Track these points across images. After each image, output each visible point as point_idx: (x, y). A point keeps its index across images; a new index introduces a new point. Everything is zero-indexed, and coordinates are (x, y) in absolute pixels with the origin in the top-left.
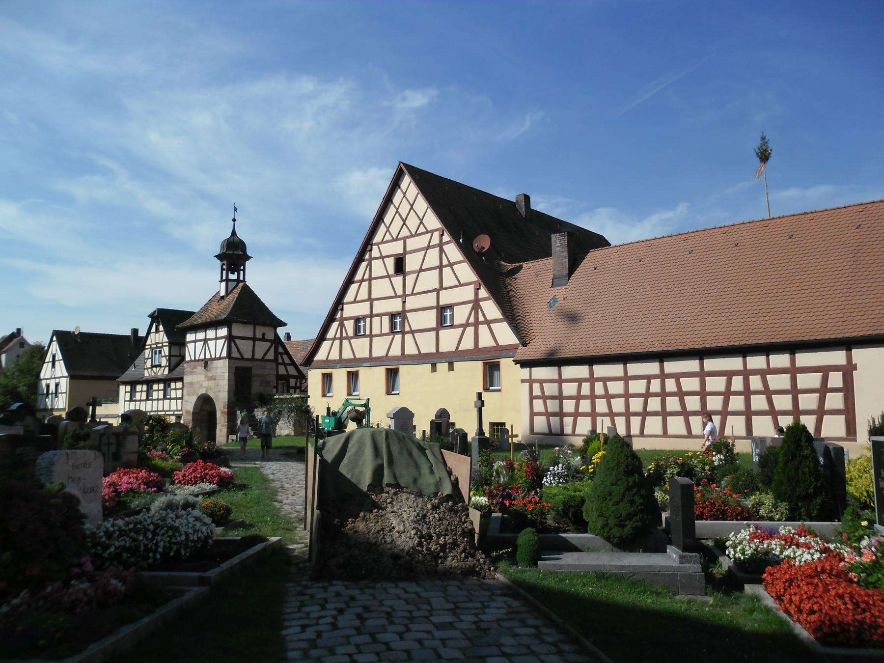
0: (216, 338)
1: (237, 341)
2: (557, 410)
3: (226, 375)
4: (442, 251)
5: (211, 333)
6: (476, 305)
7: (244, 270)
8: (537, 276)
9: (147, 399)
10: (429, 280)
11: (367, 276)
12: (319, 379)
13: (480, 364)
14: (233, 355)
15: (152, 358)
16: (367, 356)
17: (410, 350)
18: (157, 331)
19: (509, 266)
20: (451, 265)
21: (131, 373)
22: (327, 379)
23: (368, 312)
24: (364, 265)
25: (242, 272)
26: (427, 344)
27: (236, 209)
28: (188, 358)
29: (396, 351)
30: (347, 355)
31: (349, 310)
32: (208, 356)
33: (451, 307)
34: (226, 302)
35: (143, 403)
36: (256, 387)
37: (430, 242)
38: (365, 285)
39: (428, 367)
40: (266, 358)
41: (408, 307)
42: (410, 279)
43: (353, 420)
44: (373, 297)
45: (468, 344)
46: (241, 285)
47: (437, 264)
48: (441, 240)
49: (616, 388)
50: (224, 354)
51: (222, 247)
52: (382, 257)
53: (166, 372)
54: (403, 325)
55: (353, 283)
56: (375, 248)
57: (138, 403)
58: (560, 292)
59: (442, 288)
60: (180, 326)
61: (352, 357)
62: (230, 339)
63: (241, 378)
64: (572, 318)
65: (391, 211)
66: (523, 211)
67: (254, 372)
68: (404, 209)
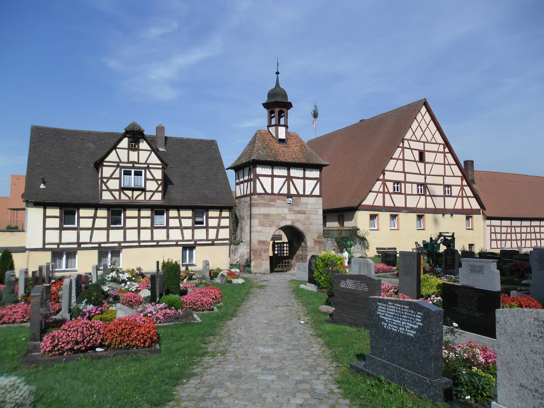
0: (304, 178)
4: (445, 156)
6: (462, 189)
12: (389, 217)
17: (430, 205)
30: (389, 203)
39: (464, 216)
40: (281, 192)
45: (459, 206)
49: (518, 230)
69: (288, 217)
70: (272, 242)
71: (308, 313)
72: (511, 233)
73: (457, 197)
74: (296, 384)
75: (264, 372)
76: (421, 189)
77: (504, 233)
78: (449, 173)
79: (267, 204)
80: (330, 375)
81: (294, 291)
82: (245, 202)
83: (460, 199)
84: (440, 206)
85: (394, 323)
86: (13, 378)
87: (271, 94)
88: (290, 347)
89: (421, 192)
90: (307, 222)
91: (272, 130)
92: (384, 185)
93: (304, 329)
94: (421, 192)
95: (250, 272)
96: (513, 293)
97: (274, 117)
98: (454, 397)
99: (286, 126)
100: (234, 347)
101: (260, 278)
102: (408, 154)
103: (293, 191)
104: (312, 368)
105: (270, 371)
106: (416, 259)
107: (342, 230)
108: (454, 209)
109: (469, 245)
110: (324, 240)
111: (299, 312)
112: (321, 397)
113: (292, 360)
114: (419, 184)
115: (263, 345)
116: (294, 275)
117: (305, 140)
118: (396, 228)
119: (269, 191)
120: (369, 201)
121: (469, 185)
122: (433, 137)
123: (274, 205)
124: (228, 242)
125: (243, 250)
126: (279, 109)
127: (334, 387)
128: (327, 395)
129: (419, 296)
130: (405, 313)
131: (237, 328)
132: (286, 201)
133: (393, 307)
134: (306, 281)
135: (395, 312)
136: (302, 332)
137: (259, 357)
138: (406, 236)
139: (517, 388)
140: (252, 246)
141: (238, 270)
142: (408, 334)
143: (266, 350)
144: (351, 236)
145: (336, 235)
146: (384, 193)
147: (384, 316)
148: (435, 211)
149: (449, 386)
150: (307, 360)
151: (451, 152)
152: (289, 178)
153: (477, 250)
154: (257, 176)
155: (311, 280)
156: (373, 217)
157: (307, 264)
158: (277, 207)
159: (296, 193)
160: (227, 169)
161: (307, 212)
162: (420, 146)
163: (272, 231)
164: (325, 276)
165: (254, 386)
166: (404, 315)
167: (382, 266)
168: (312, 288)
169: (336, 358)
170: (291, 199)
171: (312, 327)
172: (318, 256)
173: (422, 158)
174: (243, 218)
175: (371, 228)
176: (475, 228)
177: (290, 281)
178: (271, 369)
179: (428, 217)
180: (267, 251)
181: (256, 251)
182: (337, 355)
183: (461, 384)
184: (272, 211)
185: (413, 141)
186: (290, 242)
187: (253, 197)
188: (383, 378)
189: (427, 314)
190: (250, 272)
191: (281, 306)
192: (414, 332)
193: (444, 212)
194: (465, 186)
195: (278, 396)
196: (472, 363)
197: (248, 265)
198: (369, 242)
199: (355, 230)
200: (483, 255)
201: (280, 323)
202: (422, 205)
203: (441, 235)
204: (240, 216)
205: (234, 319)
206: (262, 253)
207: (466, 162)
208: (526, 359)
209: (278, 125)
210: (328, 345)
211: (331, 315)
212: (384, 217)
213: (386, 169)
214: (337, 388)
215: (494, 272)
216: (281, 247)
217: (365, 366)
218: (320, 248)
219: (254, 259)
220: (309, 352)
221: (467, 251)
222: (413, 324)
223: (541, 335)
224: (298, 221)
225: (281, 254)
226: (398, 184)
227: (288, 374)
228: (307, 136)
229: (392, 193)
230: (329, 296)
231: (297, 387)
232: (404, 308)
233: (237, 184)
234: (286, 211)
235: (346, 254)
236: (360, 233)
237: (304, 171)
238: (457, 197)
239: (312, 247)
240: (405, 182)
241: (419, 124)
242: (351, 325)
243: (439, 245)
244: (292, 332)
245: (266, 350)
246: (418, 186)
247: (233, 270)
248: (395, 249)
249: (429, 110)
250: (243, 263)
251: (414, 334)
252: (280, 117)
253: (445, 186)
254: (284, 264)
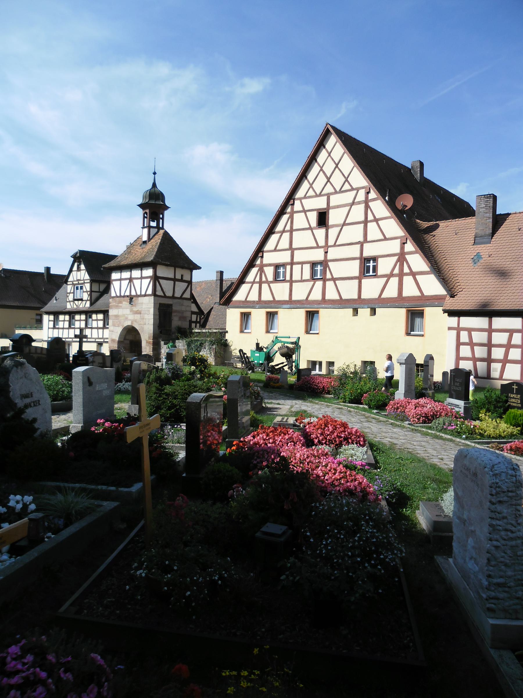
0: (142, 278)
1: (161, 281)
2: (485, 356)
3: (152, 311)
4: (367, 207)
5: (136, 273)
6: (402, 257)
7: (163, 219)
8: (456, 234)
9: (70, 327)
10: (355, 233)
11: (288, 228)
12: (238, 316)
13: (403, 311)
14: (157, 293)
15: (74, 293)
16: (287, 298)
17: (331, 294)
18: (79, 269)
19: (425, 225)
20: (376, 220)
21: (53, 304)
22: (245, 317)
23: (289, 260)
24: (285, 217)
25: (161, 220)
26: (349, 291)
28: (113, 294)
29: (316, 295)
30: (266, 296)
31: (269, 258)
32: (133, 293)
33: (375, 259)
34: (149, 246)
35: (66, 331)
36: (176, 322)
37: (355, 198)
38: (286, 235)
41: (329, 257)
42: (333, 233)
43: (283, 355)
44: (294, 247)
45: (391, 292)
46: (161, 232)
47: (362, 219)
48: (367, 197)
50: (150, 291)
51: (144, 197)
52: (305, 211)
53: (88, 304)
54: (324, 272)
55: (274, 233)
56: (297, 203)
57: (61, 331)
58: (484, 249)
59: (366, 240)
60: (106, 265)
61: (272, 299)
62: (156, 279)
63: (164, 313)
64: (502, 274)
65: (315, 169)
66: (418, 176)
67: (174, 308)
68: (329, 167)
86: (387, 507)
90: (142, 323)
173: (323, 219)
229: (271, 282)
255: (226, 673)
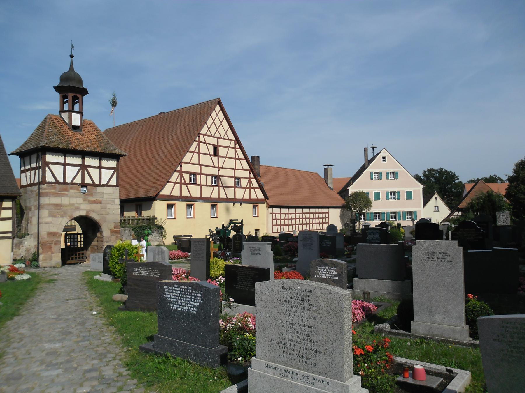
1: (50, 166)
4: (236, 151)
6: (250, 181)
16: (199, 196)
17: (223, 196)
27: (73, 47)
30: (185, 193)
39: (251, 205)
40: (74, 182)
45: (247, 197)
69: (83, 207)
70: (64, 233)
71: (102, 304)
72: (316, 218)
73: (246, 188)
74: (84, 374)
75: (49, 368)
76: (215, 180)
77: (283, 219)
78: (239, 166)
79: (58, 194)
80: (120, 360)
81: (87, 283)
82: (32, 191)
83: (248, 190)
84: (231, 196)
85: (179, 303)
87: (64, 78)
88: (80, 339)
89: (215, 183)
91: (65, 116)
92: (181, 176)
93: (96, 319)
94: (215, 183)
95: (38, 267)
96: (285, 269)
97: (67, 102)
98: (229, 361)
99: (81, 113)
100: (14, 348)
101: (50, 271)
102: (203, 148)
103: (88, 181)
104: (101, 356)
105: (57, 366)
106: (206, 244)
107: (139, 220)
108: (243, 199)
109: (255, 230)
110: (121, 229)
111: (92, 303)
112: (109, 382)
113: (81, 351)
114: (213, 176)
115: (50, 341)
116: (88, 266)
117: (102, 129)
118: (192, 217)
119: (61, 180)
120: (166, 191)
121: (255, 178)
122: (226, 134)
123: (67, 194)
124: (10, 235)
125: (29, 244)
126: (73, 95)
127: (123, 370)
128: (116, 379)
129: (208, 277)
130: (189, 294)
131: (18, 328)
132: (80, 191)
133: (178, 289)
134: (100, 272)
135: (180, 294)
136: (93, 323)
137: (44, 354)
138: (200, 224)
139: (269, 343)
140: (40, 238)
141: (23, 266)
142: (191, 312)
143: (52, 346)
144: (148, 225)
145: (133, 224)
146: (181, 183)
147: (170, 298)
148: (227, 200)
149: (224, 352)
150: (98, 349)
151: (241, 148)
152: (83, 167)
153: (261, 235)
154: (47, 164)
155: (107, 270)
156: (170, 206)
157: (102, 255)
158: (70, 197)
159: (91, 183)
160: (9, 155)
161: (103, 202)
162: (214, 141)
163: (64, 222)
164: (120, 264)
165: (36, 384)
166: (187, 295)
167: (177, 252)
168: (107, 278)
169: (127, 343)
170: (85, 189)
171: (104, 317)
172: (113, 246)
173: (215, 152)
174: (30, 209)
175: (168, 217)
176: (177, 217)
177: (83, 273)
178: (57, 364)
179: (221, 206)
180: (58, 242)
181: (45, 244)
182: (128, 340)
183: (235, 348)
184: (65, 201)
185: (208, 136)
186: (84, 233)
187: (42, 186)
188: (169, 354)
189: (207, 293)
190: (38, 267)
191: (73, 299)
192: (196, 310)
193: (234, 201)
194: (252, 178)
195: (63, 389)
196: (246, 330)
197: (35, 258)
198: (166, 230)
199: (153, 219)
200: (266, 239)
201: (70, 317)
202: (215, 195)
203: (231, 222)
204: (26, 207)
205: (16, 319)
206: (53, 245)
207: (253, 158)
208: (275, 319)
209: (72, 111)
210: (120, 332)
211: (124, 303)
212: (181, 206)
213: (183, 161)
214: (126, 371)
215: (268, 253)
216: (74, 238)
217: (153, 346)
218: (116, 238)
219: (43, 252)
220: (100, 341)
221: (252, 236)
222: (194, 302)
223: (285, 299)
224: (93, 211)
225: (74, 245)
226: (193, 176)
227: (75, 366)
228: (103, 125)
230: (123, 285)
231: (85, 377)
232: (187, 289)
233: (22, 172)
234: (80, 200)
235: (144, 243)
236: (157, 222)
237: (101, 160)
238: (246, 188)
239: (108, 237)
240: (201, 174)
241: (214, 121)
242: (143, 310)
243: (230, 231)
244: (83, 324)
245: (52, 346)
246: (212, 178)
247: (16, 266)
248: (191, 236)
249: (222, 109)
250: (30, 257)
251: (195, 311)
252: (74, 103)
253: (236, 178)
254: (78, 256)
255: (337, 278)
